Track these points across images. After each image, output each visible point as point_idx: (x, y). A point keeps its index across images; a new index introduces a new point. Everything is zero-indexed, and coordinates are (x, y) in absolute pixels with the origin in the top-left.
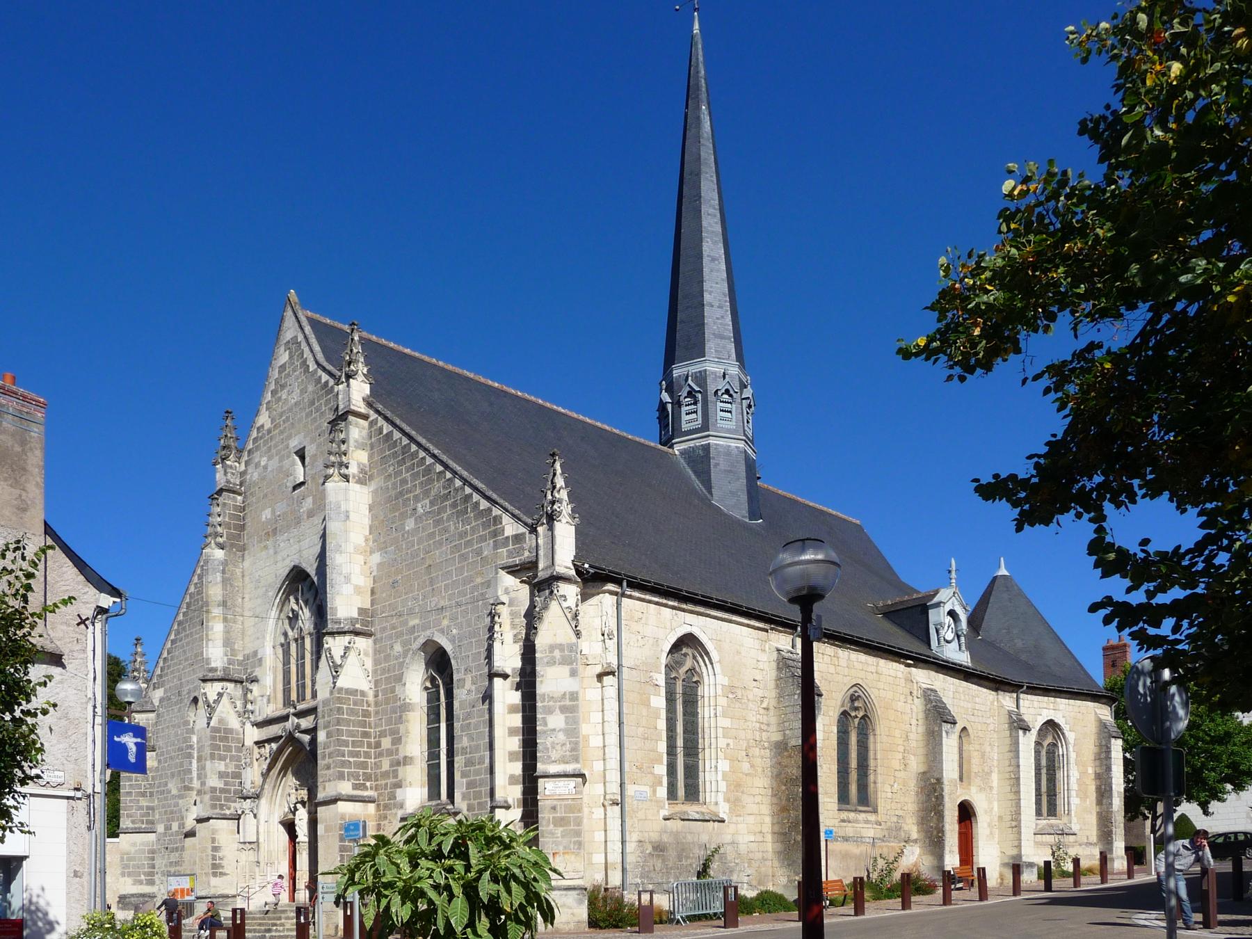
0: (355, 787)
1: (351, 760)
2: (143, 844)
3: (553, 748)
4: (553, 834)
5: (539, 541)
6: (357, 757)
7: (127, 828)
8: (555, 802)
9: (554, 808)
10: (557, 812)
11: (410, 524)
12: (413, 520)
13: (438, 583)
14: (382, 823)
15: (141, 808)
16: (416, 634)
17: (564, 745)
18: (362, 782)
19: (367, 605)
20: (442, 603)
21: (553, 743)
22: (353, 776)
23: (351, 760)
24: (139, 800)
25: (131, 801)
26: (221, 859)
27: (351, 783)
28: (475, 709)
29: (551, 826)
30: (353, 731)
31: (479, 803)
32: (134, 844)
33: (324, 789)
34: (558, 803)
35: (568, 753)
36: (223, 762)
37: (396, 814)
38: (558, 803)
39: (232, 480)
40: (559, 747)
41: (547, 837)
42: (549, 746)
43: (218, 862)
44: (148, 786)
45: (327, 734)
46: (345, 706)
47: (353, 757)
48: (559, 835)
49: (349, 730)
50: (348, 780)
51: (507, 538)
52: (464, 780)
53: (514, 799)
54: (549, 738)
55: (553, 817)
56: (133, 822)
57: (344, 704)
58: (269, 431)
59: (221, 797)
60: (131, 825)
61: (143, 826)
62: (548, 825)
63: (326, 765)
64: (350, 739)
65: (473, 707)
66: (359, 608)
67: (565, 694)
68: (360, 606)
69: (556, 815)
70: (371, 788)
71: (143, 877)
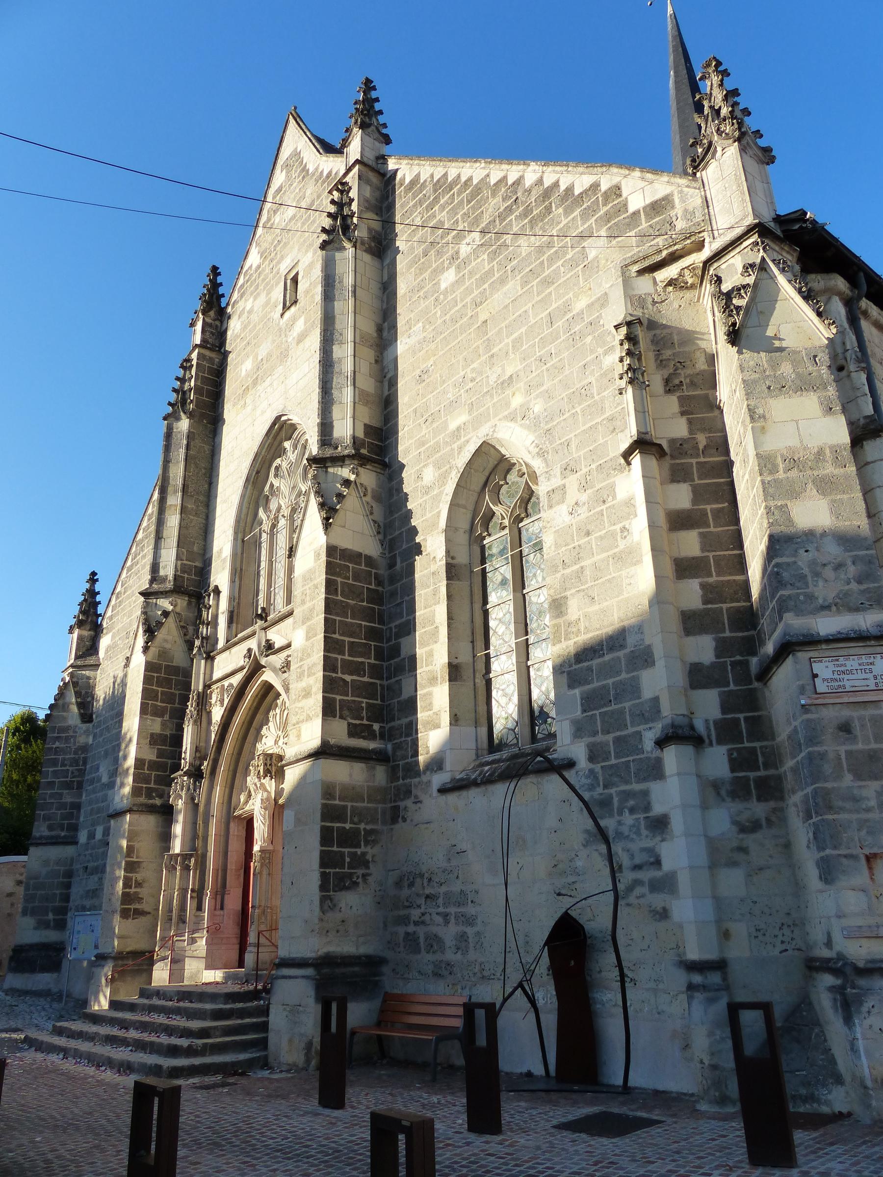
0: (353, 731)
1: (348, 678)
2: (58, 862)
3: (817, 575)
4: (856, 800)
5: (477, 681)
6: (359, 675)
7: (41, 837)
8: (846, 713)
9: (845, 728)
10: (854, 740)
11: (449, 277)
12: (452, 271)
13: (401, 737)
14: (402, 804)
15: (63, 806)
16: (463, 439)
17: (839, 567)
18: (365, 722)
19: (375, 423)
20: (510, 371)
21: (813, 563)
22: (349, 709)
23: (348, 678)
24: (61, 795)
25: (52, 796)
26: (139, 885)
27: (346, 723)
28: (592, 537)
29: (848, 780)
30: (352, 624)
31: (617, 740)
32: (46, 863)
33: (299, 736)
34: (854, 714)
35: (854, 586)
36: (159, 720)
37: (429, 782)
38: (854, 714)
39: (210, 340)
40: (828, 573)
41: (842, 809)
42: (806, 571)
43: (133, 890)
44: (76, 773)
45: (308, 633)
46: (339, 580)
47: (351, 674)
48: (873, 803)
49: (346, 624)
50: (341, 717)
51: (636, 213)
52: (577, 692)
53: (707, 721)
54: (802, 551)
55: (849, 753)
56: (50, 828)
57: (339, 575)
58: (259, 267)
59: (150, 776)
60: (46, 833)
61: (63, 834)
62: (839, 777)
63: (304, 689)
64: (347, 639)
65: (588, 534)
66: (365, 425)
67: (820, 452)
68: (367, 422)
69: (854, 747)
70: (382, 736)
71: (51, 916)
